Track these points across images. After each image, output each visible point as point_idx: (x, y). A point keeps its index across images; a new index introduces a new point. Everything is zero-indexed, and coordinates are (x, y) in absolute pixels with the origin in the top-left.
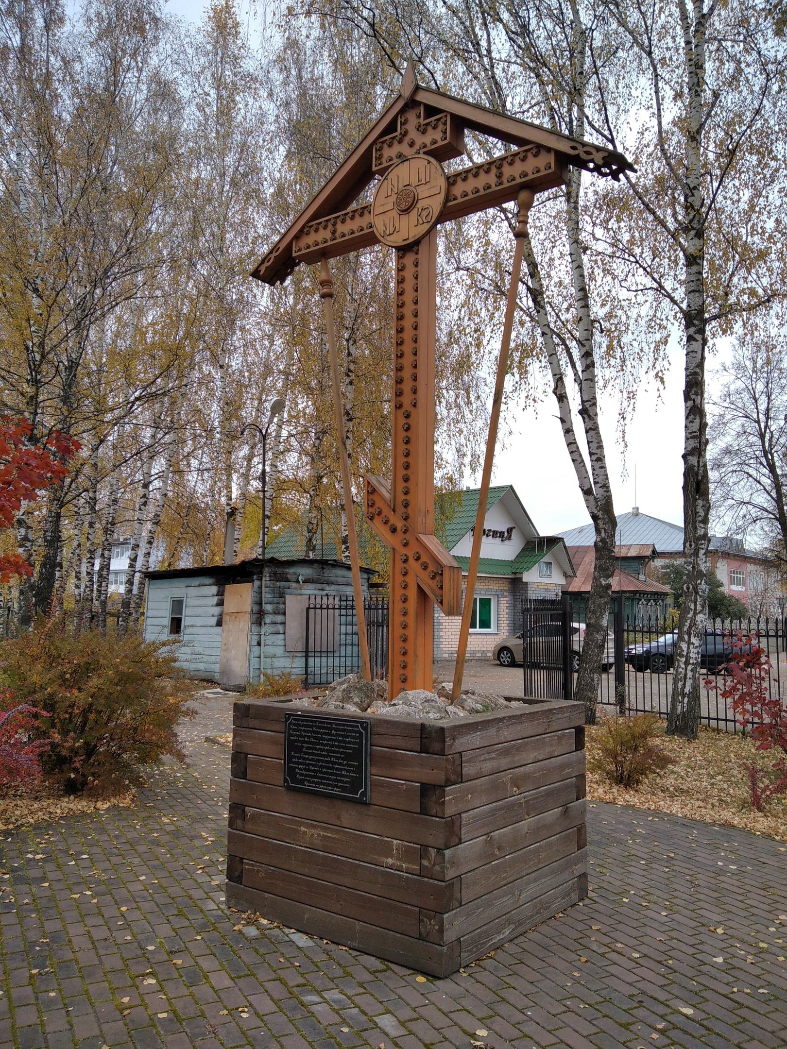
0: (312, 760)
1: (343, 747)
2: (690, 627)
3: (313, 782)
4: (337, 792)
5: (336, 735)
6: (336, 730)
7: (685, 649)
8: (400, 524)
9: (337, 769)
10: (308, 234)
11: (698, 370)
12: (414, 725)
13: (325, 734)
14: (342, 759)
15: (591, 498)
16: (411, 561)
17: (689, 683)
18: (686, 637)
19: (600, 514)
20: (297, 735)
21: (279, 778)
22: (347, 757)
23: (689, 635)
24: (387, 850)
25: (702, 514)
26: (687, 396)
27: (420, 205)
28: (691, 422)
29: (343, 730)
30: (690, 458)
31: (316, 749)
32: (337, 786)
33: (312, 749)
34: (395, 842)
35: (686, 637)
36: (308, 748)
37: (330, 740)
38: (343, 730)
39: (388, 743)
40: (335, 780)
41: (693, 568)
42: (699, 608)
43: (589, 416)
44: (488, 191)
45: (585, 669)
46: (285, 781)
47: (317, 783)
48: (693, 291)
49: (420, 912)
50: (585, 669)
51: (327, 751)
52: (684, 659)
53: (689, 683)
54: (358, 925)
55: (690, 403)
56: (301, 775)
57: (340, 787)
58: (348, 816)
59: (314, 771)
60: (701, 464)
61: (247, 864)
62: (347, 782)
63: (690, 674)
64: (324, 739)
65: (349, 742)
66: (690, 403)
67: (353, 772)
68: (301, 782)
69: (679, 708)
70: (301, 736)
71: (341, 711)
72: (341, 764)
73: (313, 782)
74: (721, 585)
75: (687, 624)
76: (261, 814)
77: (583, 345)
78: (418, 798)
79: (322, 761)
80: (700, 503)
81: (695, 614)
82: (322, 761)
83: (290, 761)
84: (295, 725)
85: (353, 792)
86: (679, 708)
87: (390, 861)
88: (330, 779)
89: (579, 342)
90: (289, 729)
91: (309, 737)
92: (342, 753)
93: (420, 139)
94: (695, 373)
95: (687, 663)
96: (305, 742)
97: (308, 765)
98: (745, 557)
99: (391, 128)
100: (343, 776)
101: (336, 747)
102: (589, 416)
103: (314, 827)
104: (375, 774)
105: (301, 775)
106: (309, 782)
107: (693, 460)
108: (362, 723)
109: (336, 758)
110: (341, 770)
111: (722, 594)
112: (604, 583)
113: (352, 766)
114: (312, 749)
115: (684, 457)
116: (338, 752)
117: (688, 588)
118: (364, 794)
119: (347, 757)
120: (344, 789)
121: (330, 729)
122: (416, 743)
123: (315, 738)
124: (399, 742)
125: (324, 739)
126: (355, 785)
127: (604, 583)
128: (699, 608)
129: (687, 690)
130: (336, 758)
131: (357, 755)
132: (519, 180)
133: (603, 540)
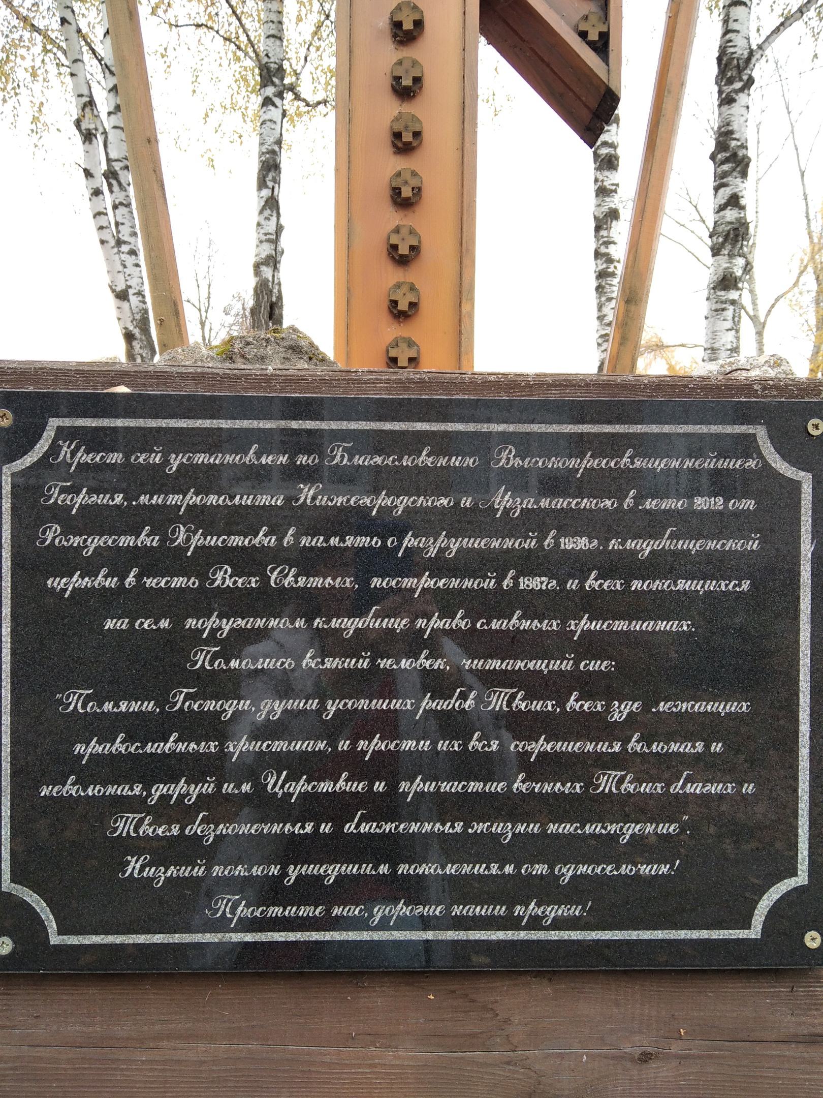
1: (592, 603)
4: (550, 924)
5: (535, 522)
6: (517, 481)
11: (276, 148)
14: (589, 686)
15: (125, 305)
19: (137, 332)
20: (118, 561)
22: (642, 671)
26: (262, 184)
28: (267, 219)
30: (264, 268)
32: (547, 890)
43: (120, 184)
47: (347, 889)
48: (273, 36)
55: (266, 193)
57: (577, 890)
60: (276, 281)
62: (641, 848)
65: (656, 566)
66: (266, 193)
67: (704, 766)
84: (94, 477)
88: (488, 850)
91: (247, 561)
92: (591, 645)
94: (273, 152)
96: (205, 601)
101: (533, 604)
102: (120, 184)
107: (267, 272)
113: (685, 726)
115: (257, 267)
116: (558, 645)
119: (642, 671)
120: (610, 902)
121: (481, 481)
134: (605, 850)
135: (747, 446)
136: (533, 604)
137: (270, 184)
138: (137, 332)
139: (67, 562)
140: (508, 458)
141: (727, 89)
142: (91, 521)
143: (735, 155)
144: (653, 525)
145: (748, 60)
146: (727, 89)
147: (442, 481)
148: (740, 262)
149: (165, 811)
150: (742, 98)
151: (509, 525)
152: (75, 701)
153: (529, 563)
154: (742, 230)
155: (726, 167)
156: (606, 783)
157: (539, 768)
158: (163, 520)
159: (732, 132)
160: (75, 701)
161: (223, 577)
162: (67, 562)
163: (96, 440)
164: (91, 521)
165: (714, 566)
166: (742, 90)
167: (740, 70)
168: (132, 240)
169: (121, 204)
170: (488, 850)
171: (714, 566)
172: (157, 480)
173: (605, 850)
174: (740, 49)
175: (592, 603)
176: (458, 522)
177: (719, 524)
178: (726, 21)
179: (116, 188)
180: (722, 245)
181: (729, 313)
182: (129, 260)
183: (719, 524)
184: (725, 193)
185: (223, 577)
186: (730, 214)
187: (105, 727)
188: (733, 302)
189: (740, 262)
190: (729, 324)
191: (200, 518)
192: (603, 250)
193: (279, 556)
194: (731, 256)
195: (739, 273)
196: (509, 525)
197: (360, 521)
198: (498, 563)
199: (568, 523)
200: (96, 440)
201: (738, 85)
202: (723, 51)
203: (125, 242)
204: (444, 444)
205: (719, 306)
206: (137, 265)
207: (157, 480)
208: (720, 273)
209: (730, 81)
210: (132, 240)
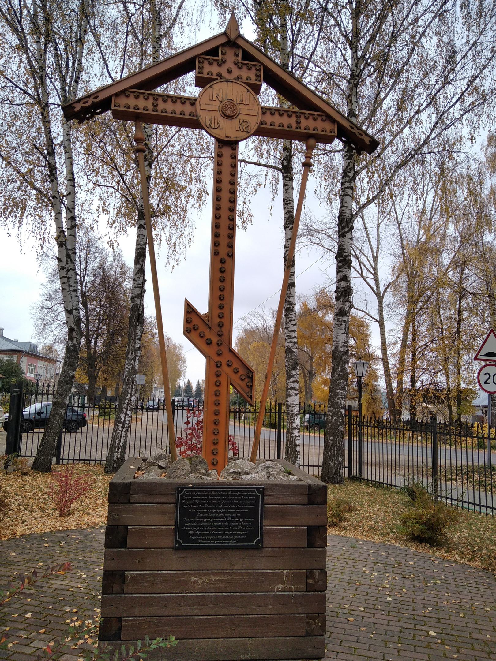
0: (207, 522)
1: (239, 508)
2: (128, 404)
3: (209, 539)
4: (233, 543)
5: (233, 500)
6: (232, 495)
7: (123, 419)
8: (215, 340)
9: (233, 526)
10: (127, 96)
12: (302, 486)
13: (222, 500)
14: (238, 517)
15: (71, 316)
16: (224, 367)
17: (123, 439)
18: (125, 411)
19: (75, 327)
20: (190, 504)
21: (169, 541)
22: (243, 515)
23: (127, 409)
24: (278, 578)
25: (139, 334)
27: (241, 117)
29: (239, 495)
30: (136, 299)
31: (211, 513)
32: (233, 539)
33: (207, 513)
34: (285, 571)
35: (125, 411)
36: (202, 513)
37: (226, 504)
38: (239, 495)
39: (280, 501)
40: (230, 535)
41: (132, 367)
42: (133, 392)
43: (71, 260)
44: (272, 127)
45: (50, 434)
46: (177, 542)
47: (213, 539)
49: (306, 617)
50: (50, 434)
51: (223, 513)
52: (121, 425)
53: (123, 439)
54: (249, 641)
56: (193, 535)
58: (240, 561)
59: (209, 530)
61: (126, 621)
62: (243, 535)
63: (124, 434)
64: (220, 504)
65: (246, 504)
66: (138, 266)
67: (249, 526)
68: (196, 541)
69: (116, 456)
70: (195, 504)
71: (200, 481)
72: (238, 522)
73: (209, 539)
74: (23, 373)
75: (126, 403)
76: (144, 575)
77: (71, 212)
78: (305, 537)
79: (218, 522)
80: (139, 328)
81: (131, 396)
82: (218, 522)
83: (182, 525)
85: (249, 540)
86: (116, 456)
87: (280, 586)
88: (227, 535)
89: (67, 208)
90: (182, 499)
91: (203, 504)
92: (239, 513)
93: (236, 72)
95: (123, 427)
96: (199, 508)
97: (203, 526)
98: (37, 356)
99: (214, 52)
100: (240, 530)
101: (232, 508)
102: (71, 260)
103: (206, 575)
104: (268, 525)
105: (193, 535)
106: (203, 540)
108: (258, 489)
109: (232, 517)
110: (237, 526)
111: (25, 379)
112: (71, 374)
114: (207, 513)
117: (128, 380)
118: (260, 541)
119: (243, 515)
120: (239, 541)
121: (228, 495)
122: (304, 498)
123: (210, 504)
124: (292, 499)
125: (220, 504)
126: (251, 535)
127: (71, 374)
128: (133, 392)
129: (121, 444)
130: (232, 517)
131: (254, 513)
132: (311, 131)
133: (74, 346)
134: (239, 535)
135: (254, 491)
136: (232, 508)
137: (141, 263)
138: (75, 327)
139: (185, 504)
140: (230, 493)
141: (342, 231)
142: (188, 500)
143: (345, 259)
144: (245, 500)
145: (351, 219)
146: (342, 231)
147: (224, 495)
148: (348, 304)
149: (194, 531)
150: (348, 235)
151: (230, 500)
152: (185, 519)
153: (232, 504)
154: (348, 291)
155: (341, 264)
156: (239, 528)
157: (233, 526)
158: (195, 500)
159: (344, 249)
160: (185, 519)
161: (201, 506)
162: (185, 504)
163: (188, 491)
164: (188, 500)
165: (250, 504)
166: (348, 232)
167: (347, 223)
168: (75, 285)
169: (71, 269)
170: (227, 535)
171: (250, 504)
172: (195, 496)
173: (239, 535)
174: (347, 214)
175: (239, 508)
176: (224, 500)
177: (251, 500)
178: (342, 202)
179: (69, 262)
180: (340, 297)
181: (343, 326)
182: (74, 294)
183: (251, 500)
184: (341, 274)
185: (201, 506)
186: (343, 284)
187: (188, 522)
188: (345, 322)
189: (348, 304)
190: (343, 331)
191: (199, 500)
192: (288, 299)
193: (206, 503)
194: (344, 302)
195: (347, 309)
196: (230, 500)
197: (214, 500)
198: (229, 504)
199: (236, 500)
200: (188, 491)
201: (347, 229)
202: (341, 213)
203: (72, 286)
204: (224, 491)
205: (339, 323)
206: (77, 296)
207: (195, 496)
208: (339, 308)
209: (343, 228)
210: (75, 285)
